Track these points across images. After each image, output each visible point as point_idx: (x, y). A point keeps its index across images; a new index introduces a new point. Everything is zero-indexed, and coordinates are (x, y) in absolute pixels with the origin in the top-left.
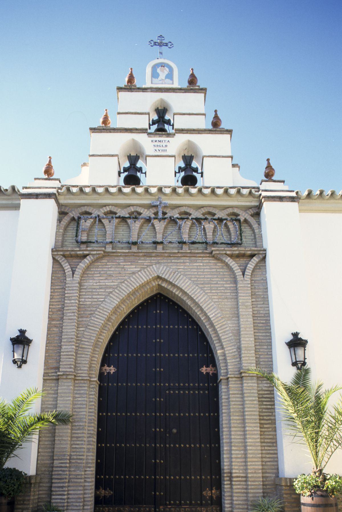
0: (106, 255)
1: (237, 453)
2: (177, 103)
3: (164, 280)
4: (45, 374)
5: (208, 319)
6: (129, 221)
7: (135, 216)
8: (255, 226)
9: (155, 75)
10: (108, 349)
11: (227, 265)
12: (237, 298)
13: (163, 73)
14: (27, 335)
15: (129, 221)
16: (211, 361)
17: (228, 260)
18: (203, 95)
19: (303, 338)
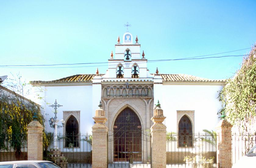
0: (114, 99)
1: (145, 147)
2: (133, 49)
3: (128, 105)
4: (33, 103)
5: (139, 115)
6: (120, 89)
7: (121, 87)
8: (152, 89)
9: (126, 39)
10: (115, 122)
11: (144, 101)
12: (146, 110)
13: (128, 38)
15: (120, 89)
16: (140, 125)
17: (144, 100)
18: (140, 46)
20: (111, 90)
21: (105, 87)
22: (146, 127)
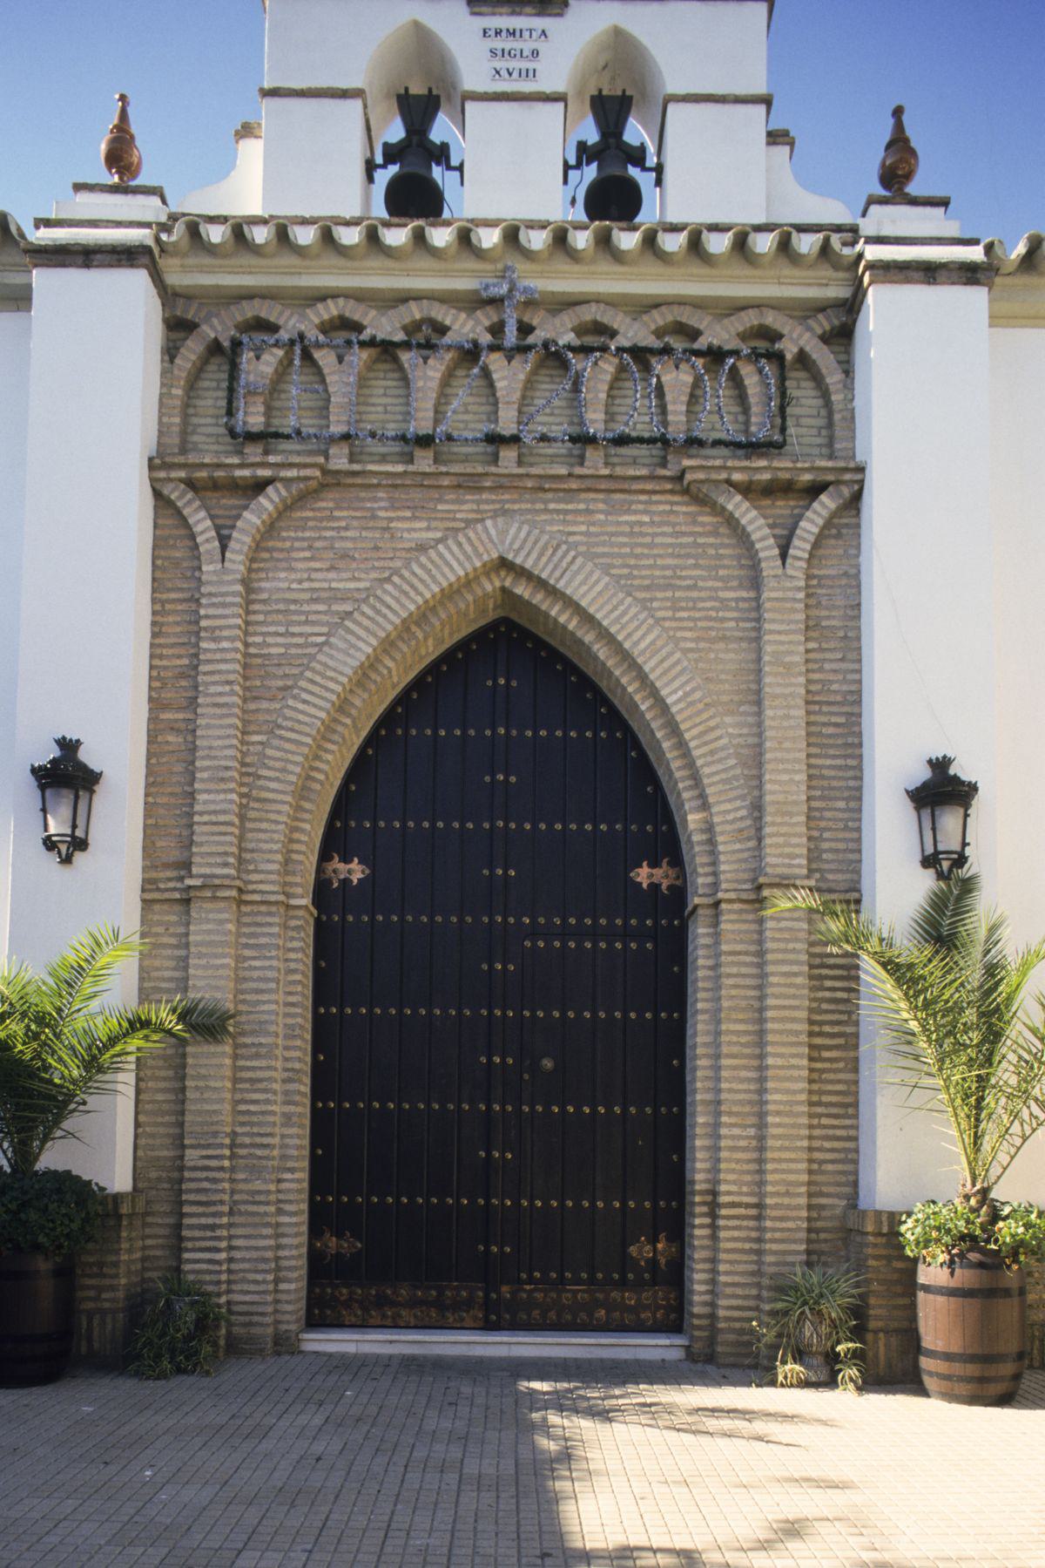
0: (332, 481)
3: (522, 573)
6: (405, 357)
8: (833, 378)
10: (342, 806)
11: (731, 522)
12: (757, 639)
14: (84, 755)
15: (405, 357)
16: (667, 844)
17: (736, 504)
19: (964, 777)
20: (285, 367)
21: (208, 332)
22: (758, 870)
